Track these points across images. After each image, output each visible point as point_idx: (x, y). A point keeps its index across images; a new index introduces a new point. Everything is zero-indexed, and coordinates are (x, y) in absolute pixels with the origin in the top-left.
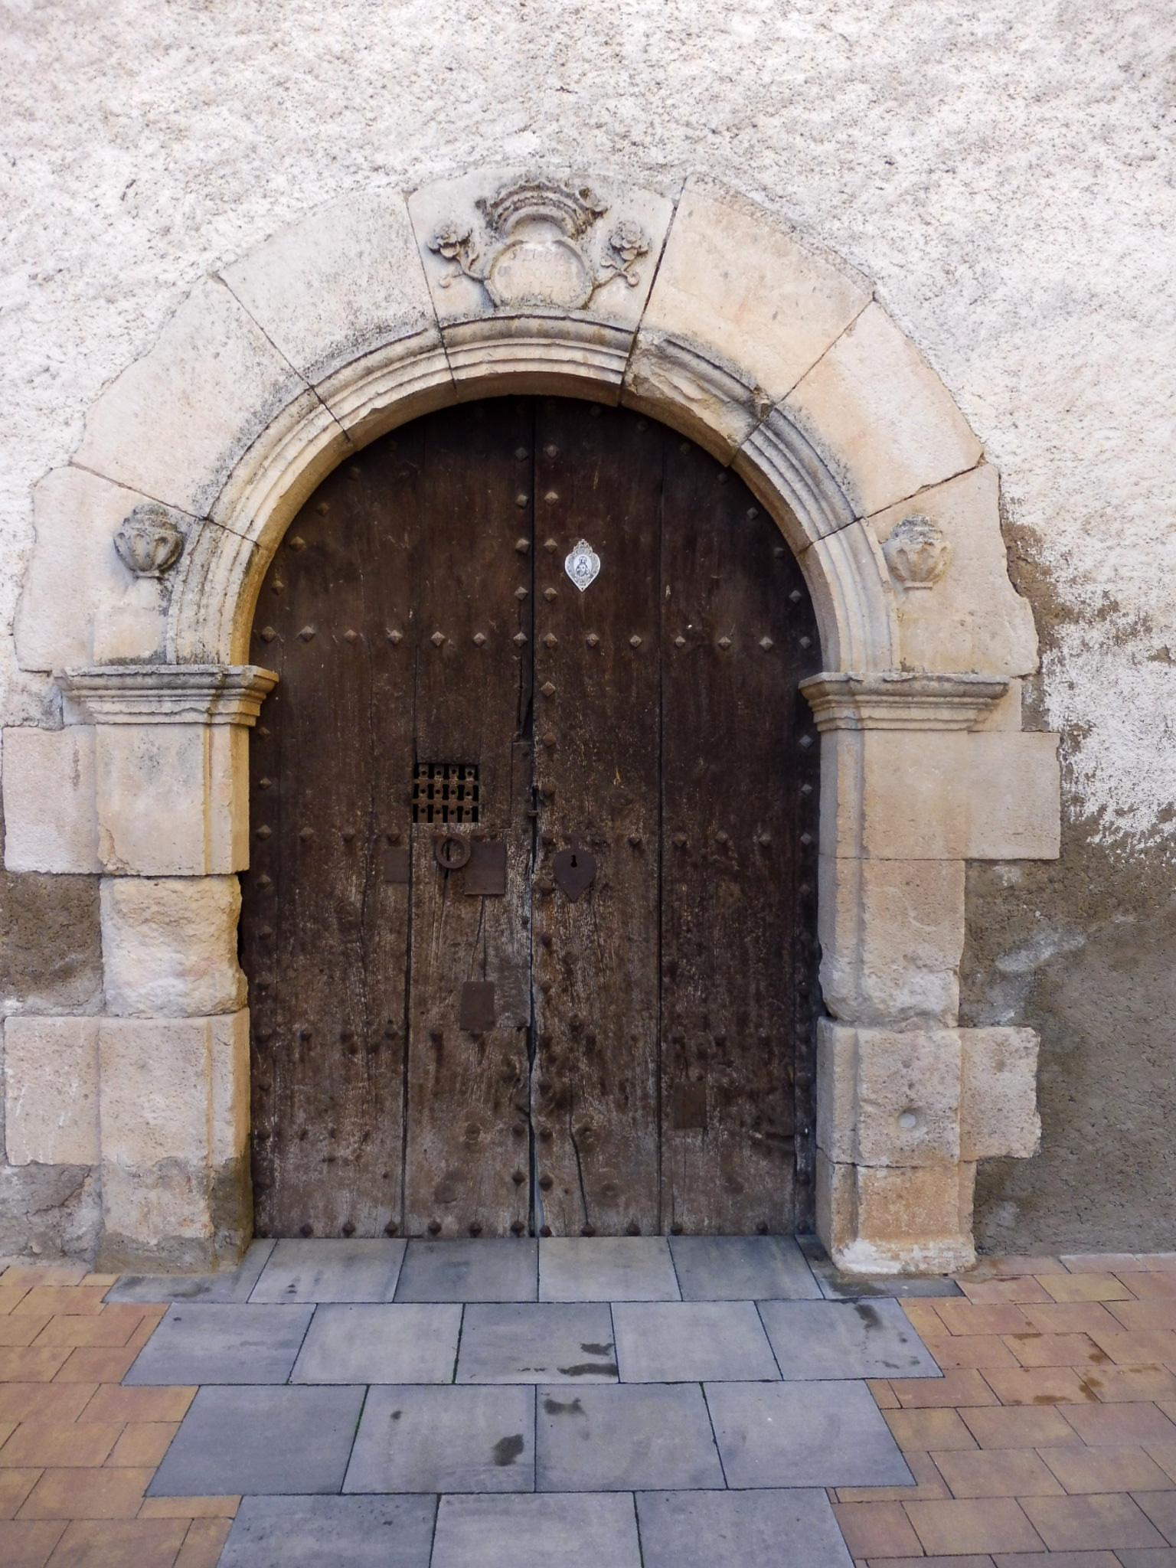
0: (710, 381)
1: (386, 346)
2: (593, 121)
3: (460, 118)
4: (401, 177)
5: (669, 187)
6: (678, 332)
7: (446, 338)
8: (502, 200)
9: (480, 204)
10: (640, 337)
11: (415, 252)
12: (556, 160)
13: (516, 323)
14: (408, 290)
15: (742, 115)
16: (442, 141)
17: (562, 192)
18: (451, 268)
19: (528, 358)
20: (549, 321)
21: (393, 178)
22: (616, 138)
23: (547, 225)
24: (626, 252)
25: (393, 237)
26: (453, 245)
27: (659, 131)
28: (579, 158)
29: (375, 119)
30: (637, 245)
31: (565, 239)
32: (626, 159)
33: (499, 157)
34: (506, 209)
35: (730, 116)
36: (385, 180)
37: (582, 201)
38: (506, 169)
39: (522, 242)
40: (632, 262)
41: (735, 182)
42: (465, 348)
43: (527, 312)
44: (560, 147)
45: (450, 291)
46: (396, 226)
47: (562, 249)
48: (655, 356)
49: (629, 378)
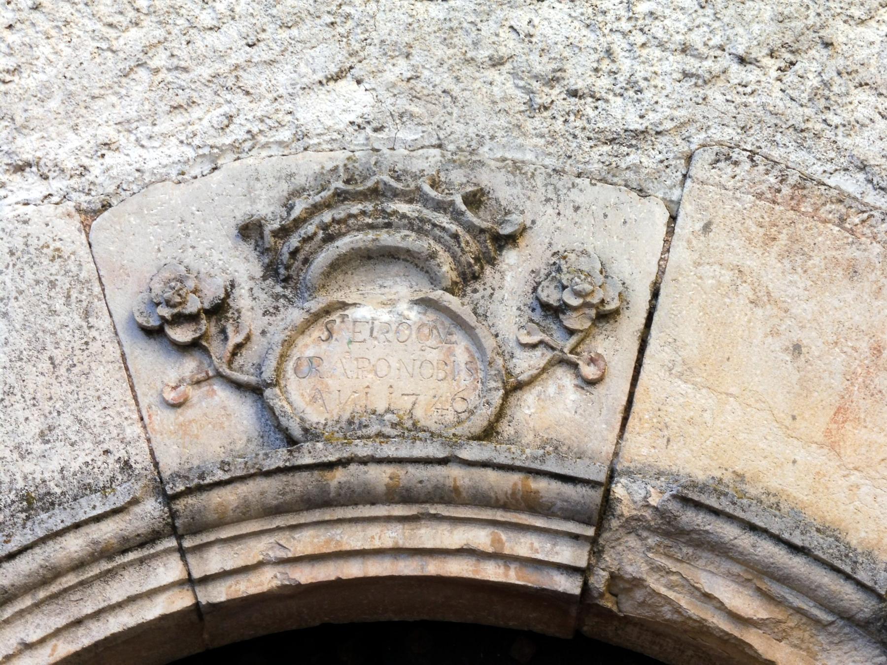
0: (785, 580)
1: (43, 540)
2: (483, 54)
3: (200, 60)
4: (74, 182)
5: (656, 176)
6: (701, 477)
7: (182, 515)
8: (298, 223)
9: (249, 230)
10: (618, 490)
11: (108, 335)
12: (408, 134)
13: (339, 476)
14: (92, 415)
15: (798, 25)
16: (163, 107)
17: (426, 200)
18: (189, 365)
19: (368, 548)
20: (411, 469)
21: (57, 185)
22: (536, 85)
23: (396, 268)
24: (573, 315)
25: (59, 304)
26: (193, 318)
27: (625, 64)
28: (459, 128)
29: (17, 70)
30: (595, 300)
31: (438, 294)
32: (559, 125)
33: (285, 135)
34: (308, 239)
35: (774, 27)
36: (38, 189)
37: (470, 216)
38: (302, 158)
39: (344, 305)
40: (586, 334)
41: (797, 157)
42: (224, 534)
43: (362, 449)
44: (414, 109)
45: (189, 413)
46: (64, 282)
47: (431, 317)
48: (655, 531)
49: (599, 580)
